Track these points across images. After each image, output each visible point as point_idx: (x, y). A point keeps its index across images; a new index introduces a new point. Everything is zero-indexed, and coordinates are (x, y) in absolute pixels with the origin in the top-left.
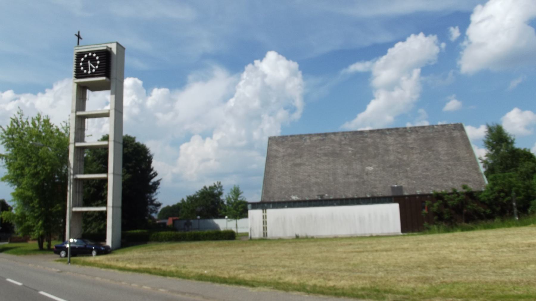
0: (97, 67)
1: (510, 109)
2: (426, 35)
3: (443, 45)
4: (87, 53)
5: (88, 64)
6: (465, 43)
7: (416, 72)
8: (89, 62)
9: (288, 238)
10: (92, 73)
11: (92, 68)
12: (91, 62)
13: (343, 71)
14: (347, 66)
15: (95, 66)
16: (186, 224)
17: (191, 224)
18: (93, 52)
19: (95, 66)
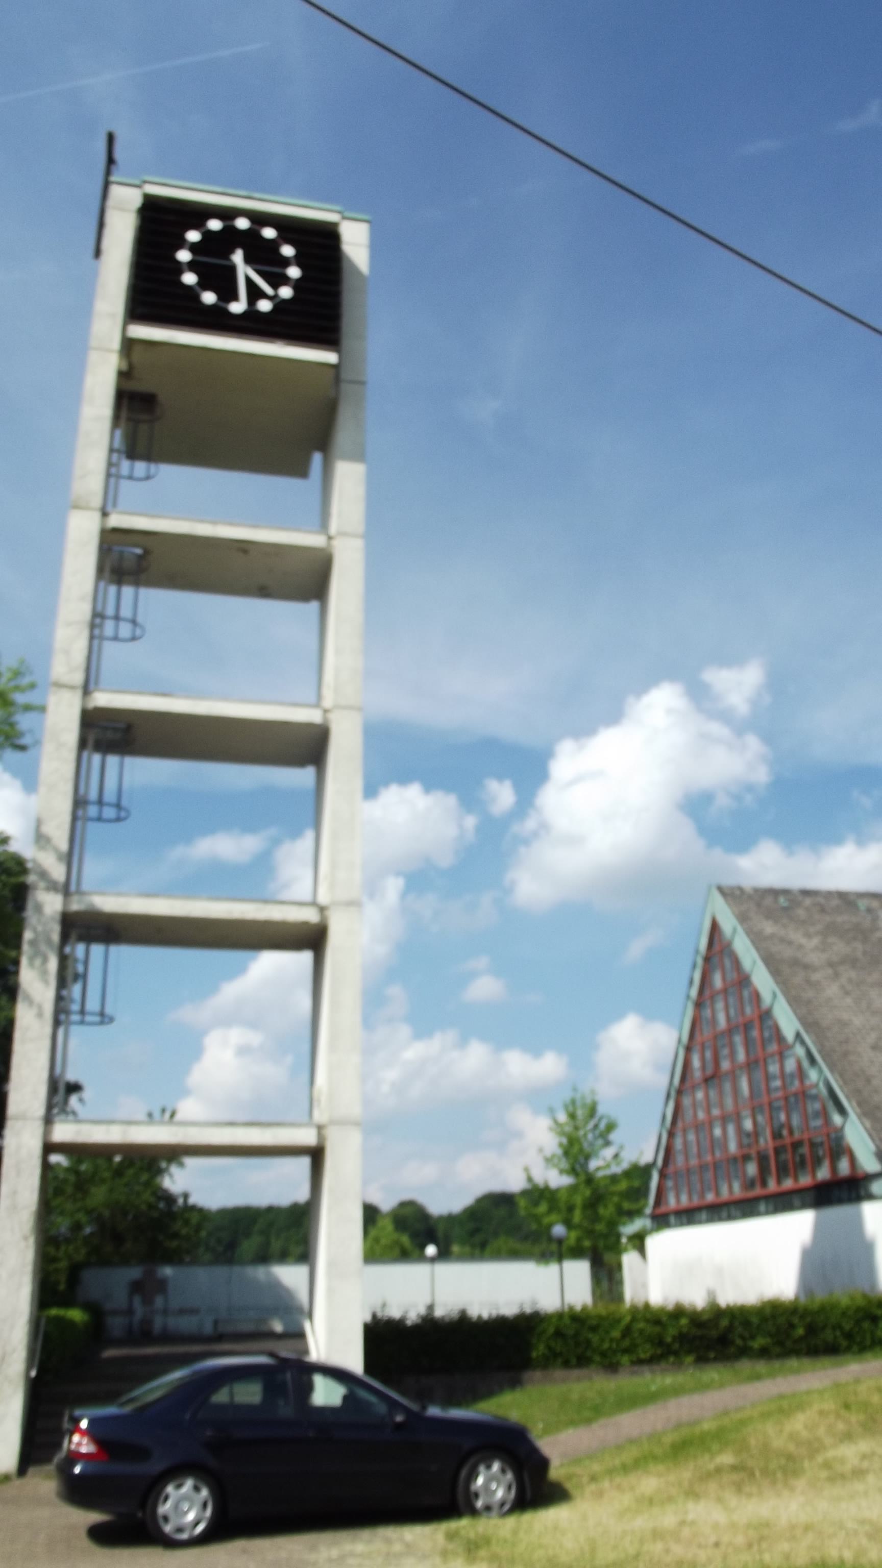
0: (286, 292)
1: (618, 1015)
2: (429, 787)
3: (470, 822)
4: (228, 214)
5: (233, 269)
6: (530, 824)
7: (393, 887)
8: (238, 257)
9: (793, 1362)
10: (251, 314)
11: (255, 293)
12: (248, 260)
13: (178, 852)
14: (189, 835)
15: (275, 286)
16: (137, 1287)
17: (162, 1286)
18: (260, 219)
19: (275, 286)
